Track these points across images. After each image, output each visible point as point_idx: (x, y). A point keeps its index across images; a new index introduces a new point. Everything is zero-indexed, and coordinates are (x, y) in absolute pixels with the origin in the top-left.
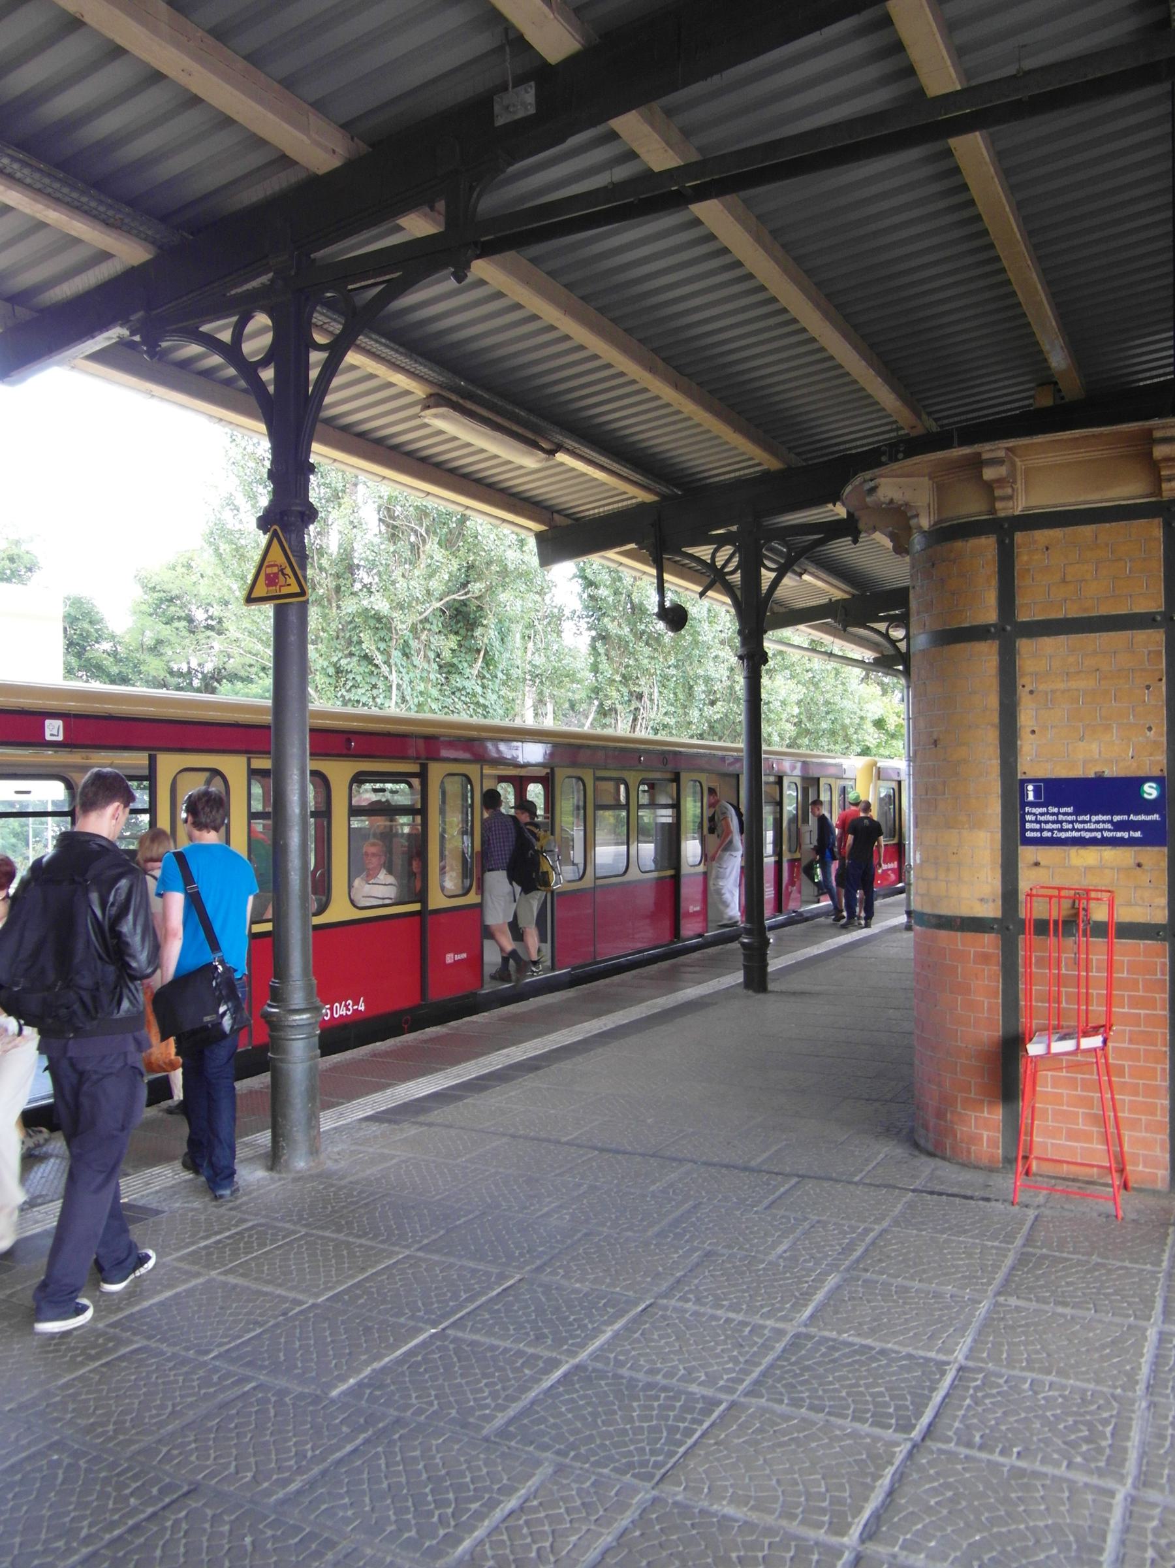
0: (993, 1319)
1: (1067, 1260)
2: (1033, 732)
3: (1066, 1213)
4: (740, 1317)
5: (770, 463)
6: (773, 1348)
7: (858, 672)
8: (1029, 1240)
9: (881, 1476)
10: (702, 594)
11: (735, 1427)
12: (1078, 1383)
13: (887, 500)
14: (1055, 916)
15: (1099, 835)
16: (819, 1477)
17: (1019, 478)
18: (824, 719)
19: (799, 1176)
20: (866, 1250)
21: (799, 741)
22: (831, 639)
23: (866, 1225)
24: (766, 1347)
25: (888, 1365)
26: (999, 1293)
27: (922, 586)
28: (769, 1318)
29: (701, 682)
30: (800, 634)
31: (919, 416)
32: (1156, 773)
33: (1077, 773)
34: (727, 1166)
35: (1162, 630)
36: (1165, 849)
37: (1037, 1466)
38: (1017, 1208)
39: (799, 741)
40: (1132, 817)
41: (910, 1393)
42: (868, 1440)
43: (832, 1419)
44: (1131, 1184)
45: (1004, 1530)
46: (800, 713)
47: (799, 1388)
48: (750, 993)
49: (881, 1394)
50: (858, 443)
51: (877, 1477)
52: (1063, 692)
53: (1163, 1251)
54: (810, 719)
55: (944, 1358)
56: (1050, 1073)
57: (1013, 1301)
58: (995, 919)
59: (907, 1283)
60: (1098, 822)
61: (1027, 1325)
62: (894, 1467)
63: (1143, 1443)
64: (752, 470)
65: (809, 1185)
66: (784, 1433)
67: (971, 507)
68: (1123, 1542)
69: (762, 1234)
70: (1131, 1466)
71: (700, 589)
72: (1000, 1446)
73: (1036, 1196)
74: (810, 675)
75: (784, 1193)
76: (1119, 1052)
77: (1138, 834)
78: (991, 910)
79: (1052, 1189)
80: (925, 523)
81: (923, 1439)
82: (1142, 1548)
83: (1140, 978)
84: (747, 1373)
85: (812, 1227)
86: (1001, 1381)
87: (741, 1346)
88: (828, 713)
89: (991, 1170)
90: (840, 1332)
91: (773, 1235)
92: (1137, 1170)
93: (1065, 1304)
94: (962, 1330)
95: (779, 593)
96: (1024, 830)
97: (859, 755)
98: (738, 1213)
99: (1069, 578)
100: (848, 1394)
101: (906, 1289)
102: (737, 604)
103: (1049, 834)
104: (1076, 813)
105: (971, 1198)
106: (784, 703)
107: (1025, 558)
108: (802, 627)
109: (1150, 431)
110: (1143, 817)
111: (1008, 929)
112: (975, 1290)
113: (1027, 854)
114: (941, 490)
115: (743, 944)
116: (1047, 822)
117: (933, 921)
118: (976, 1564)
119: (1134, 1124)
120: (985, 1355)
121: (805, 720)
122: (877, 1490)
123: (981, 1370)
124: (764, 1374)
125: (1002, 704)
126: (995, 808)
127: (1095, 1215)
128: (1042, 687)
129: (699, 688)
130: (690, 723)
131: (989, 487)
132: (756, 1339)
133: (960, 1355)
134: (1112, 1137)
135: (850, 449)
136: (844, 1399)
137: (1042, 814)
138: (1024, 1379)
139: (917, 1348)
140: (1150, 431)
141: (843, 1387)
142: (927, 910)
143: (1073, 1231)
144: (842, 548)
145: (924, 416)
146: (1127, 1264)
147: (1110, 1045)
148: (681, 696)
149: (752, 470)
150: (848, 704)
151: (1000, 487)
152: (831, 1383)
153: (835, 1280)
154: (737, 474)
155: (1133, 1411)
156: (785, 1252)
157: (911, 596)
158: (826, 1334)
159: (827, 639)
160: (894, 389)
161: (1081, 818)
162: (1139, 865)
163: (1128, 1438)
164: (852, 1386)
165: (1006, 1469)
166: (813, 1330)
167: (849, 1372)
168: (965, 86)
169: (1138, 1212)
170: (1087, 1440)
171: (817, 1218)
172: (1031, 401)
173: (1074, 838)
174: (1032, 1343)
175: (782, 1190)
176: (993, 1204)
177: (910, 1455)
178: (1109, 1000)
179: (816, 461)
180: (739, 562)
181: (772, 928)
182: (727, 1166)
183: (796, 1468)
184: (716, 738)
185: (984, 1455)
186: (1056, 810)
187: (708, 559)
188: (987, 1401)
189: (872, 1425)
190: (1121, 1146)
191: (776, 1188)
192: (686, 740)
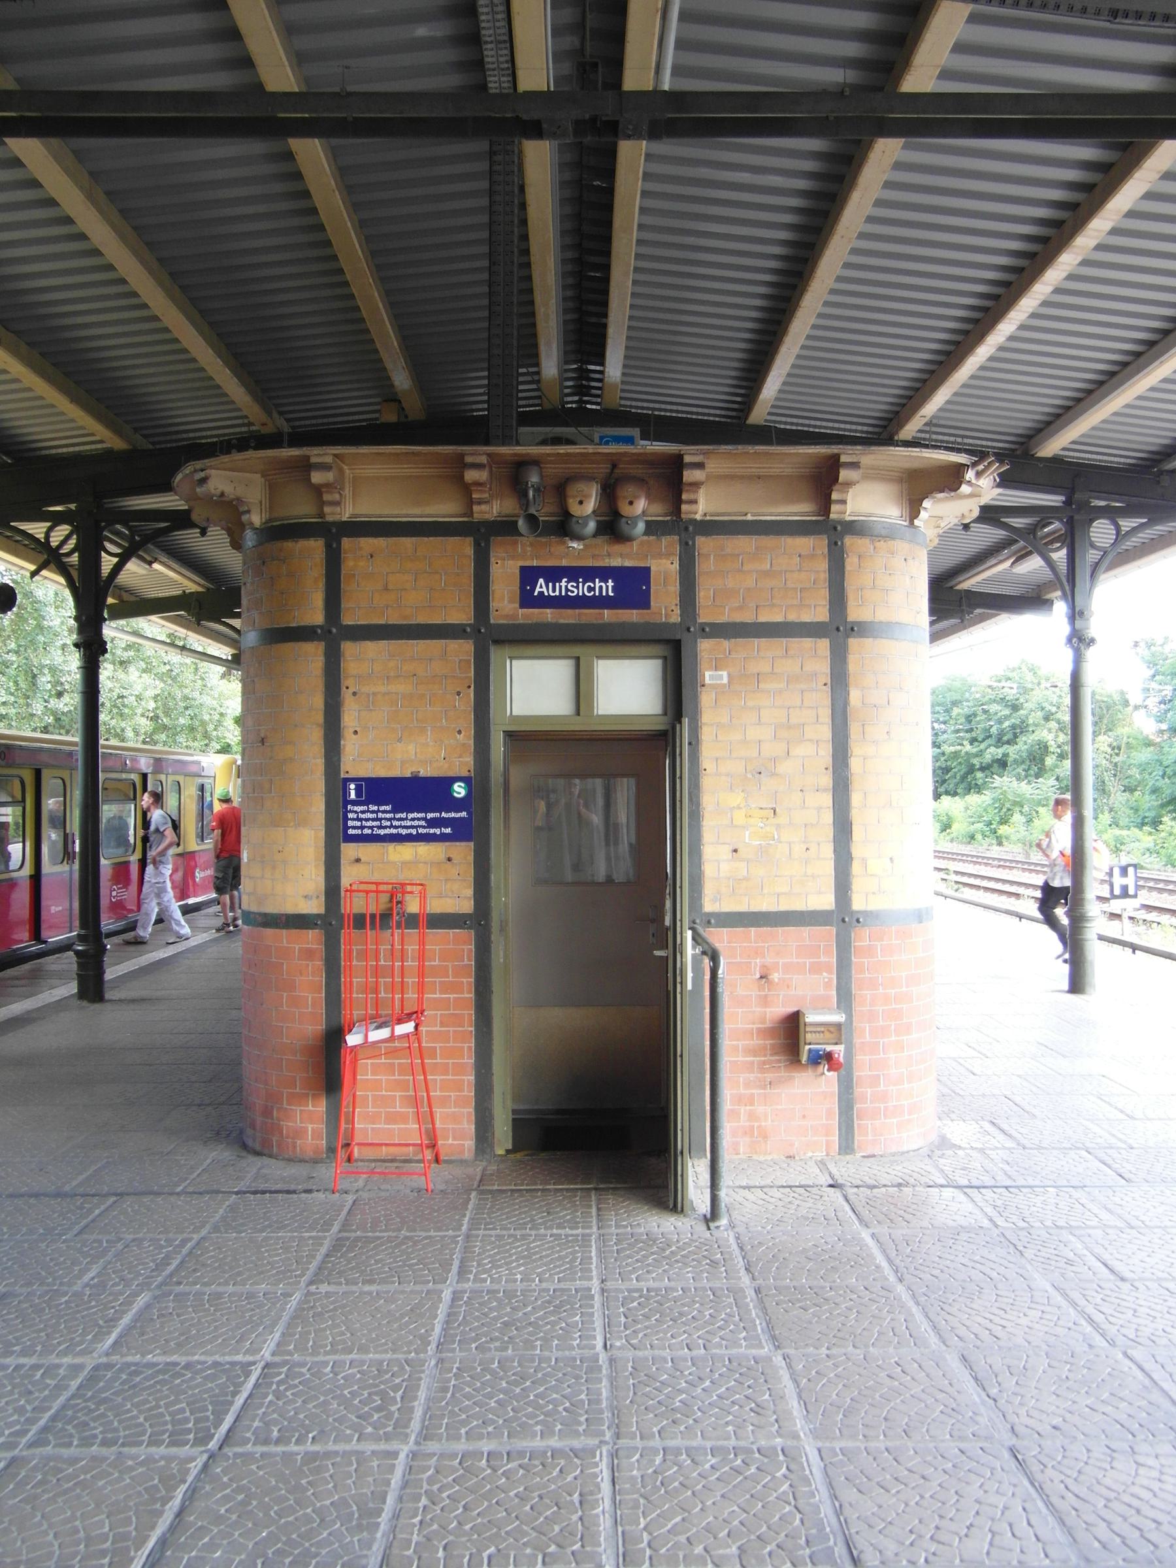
0: (304, 1309)
1: (379, 1238)
2: (356, 732)
3: (383, 1194)
4: (33, 1360)
5: (116, 443)
6: (66, 1387)
7: (221, 669)
8: (345, 1227)
9: (171, 1498)
10: (34, 574)
11: (11, 1486)
12: (377, 1356)
13: (218, 492)
14: (372, 909)
15: (414, 832)
16: (104, 1516)
17: (347, 485)
18: (182, 714)
19: (116, 1195)
20: (182, 1262)
21: (156, 737)
22: (184, 631)
23: (185, 1235)
24: (59, 1388)
25: (192, 1379)
26: (311, 1283)
27: (253, 583)
28: (66, 1355)
29: (46, 671)
30: (154, 626)
31: (270, 414)
32: (465, 774)
33: (396, 772)
34: (36, 1195)
35: (471, 642)
36: (472, 844)
37: (331, 1447)
38: (337, 1195)
39: (156, 737)
40: (443, 815)
41: (211, 1403)
42: (163, 1463)
43: (126, 1450)
44: (442, 1157)
45: (291, 1519)
46: (157, 708)
47: (92, 1425)
48: (85, 1003)
49: (182, 1411)
50: (209, 433)
51: (165, 1500)
52: (384, 694)
53: (465, 1215)
54: (167, 714)
55: (251, 1359)
56: (369, 1061)
57: (324, 1288)
58: (318, 915)
59: (221, 1289)
60: (413, 819)
61: (335, 1309)
62: (187, 1485)
63: (428, 1399)
64: (93, 447)
65: (129, 1200)
66: (69, 1478)
67: (300, 509)
68: (400, 1499)
69: (69, 1262)
70: (415, 1425)
71: (33, 568)
72: (297, 1435)
73: (356, 1181)
74: (168, 667)
75: (99, 1215)
76: (433, 1036)
77: (448, 830)
78: (315, 907)
79: (372, 1172)
80: (256, 519)
81: (220, 1448)
82: (417, 1498)
83: (450, 964)
84: (31, 1421)
85: (127, 1246)
86: (304, 1370)
87: (30, 1393)
88: (186, 708)
89: (316, 1162)
90: (143, 1355)
91: (81, 1263)
92: (447, 1143)
93: (371, 1282)
94: (270, 1328)
95: (123, 578)
96: (346, 828)
97: (219, 752)
98: (43, 1245)
99: (390, 587)
100: (146, 1419)
101: (219, 1295)
102: (71, 584)
103: (369, 831)
104: (394, 811)
105: (294, 1192)
106: (139, 698)
107: (351, 563)
108: (153, 618)
109: (461, 456)
110: (453, 815)
111: (331, 924)
112: (288, 1284)
113: (349, 851)
114: (272, 489)
115: (77, 953)
116: (367, 820)
117: (260, 919)
118: (259, 1562)
119: (444, 1101)
120: (292, 1347)
121: (161, 715)
122: (165, 1515)
123: (285, 1363)
124: (54, 1419)
125: (327, 704)
126: (318, 806)
127: (408, 1191)
128: (365, 689)
129: (45, 680)
130: (33, 715)
131: (318, 490)
132: (48, 1381)
133: (266, 1353)
134: (426, 1118)
135: (200, 438)
136: (141, 1425)
137: (363, 812)
138: (326, 1363)
139: (224, 1355)
140: (461, 456)
141: (140, 1412)
142: (254, 908)
143: (387, 1209)
144: (189, 538)
145: (275, 415)
146: (432, 1233)
147: (423, 1029)
148: (23, 685)
149: (93, 447)
150: (207, 700)
151: (328, 492)
152: (129, 1411)
153: (146, 1299)
154: (77, 449)
155: (423, 1372)
156: (93, 1278)
157: (243, 592)
158: (129, 1359)
159: (181, 632)
160: (243, 383)
161: (398, 816)
162: (449, 859)
163: (415, 1398)
164: (151, 1409)
165: (299, 1457)
166: (115, 1358)
167: (149, 1395)
168: (304, 90)
169: (446, 1182)
170: (378, 1409)
171: (131, 1237)
172: (377, 415)
173: (391, 835)
174: (338, 1326)
175: (97, 1212)
176: (315, 1194)
177: (206, 1466)
178: (421, 988)
179: (163, 446)
180: (77, 545)
181: (111, 935)
182: (36, 1195)
183: (78, 1514)
184: (63, 731)
185: (280, 1449)
186: (375, 808)
187: (41, 537)
188: (288, 1393)
189: (169, 1445)
190: (433, 1123)
191: (90, 1211)
192: (29, 734)
